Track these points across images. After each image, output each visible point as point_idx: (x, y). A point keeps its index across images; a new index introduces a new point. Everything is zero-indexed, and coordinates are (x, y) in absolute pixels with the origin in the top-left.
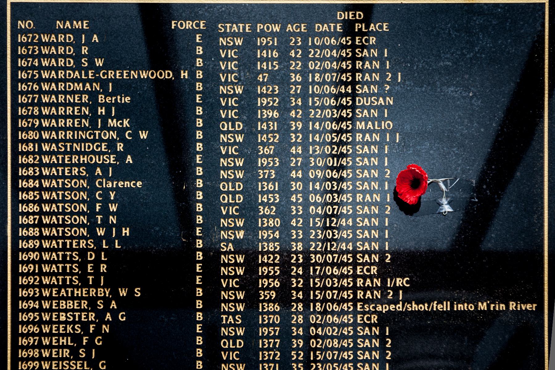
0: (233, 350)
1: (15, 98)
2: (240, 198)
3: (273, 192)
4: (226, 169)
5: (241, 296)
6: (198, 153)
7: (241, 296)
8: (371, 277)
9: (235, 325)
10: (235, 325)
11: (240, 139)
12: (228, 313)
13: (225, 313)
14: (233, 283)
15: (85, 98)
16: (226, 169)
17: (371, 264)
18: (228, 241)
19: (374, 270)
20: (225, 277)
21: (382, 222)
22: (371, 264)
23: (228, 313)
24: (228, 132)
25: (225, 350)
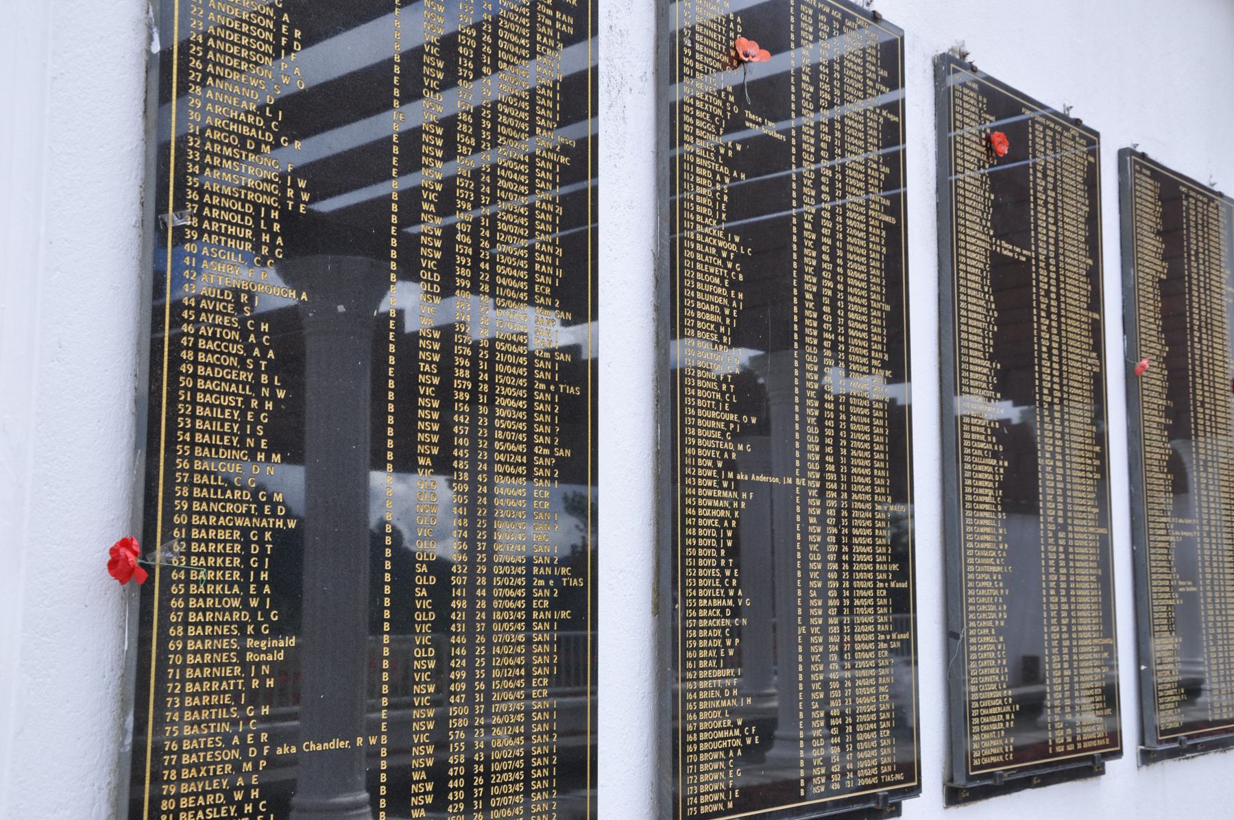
0: (426, 622)
1: (157, 380)
2: (432, 616)
3: (464, 424)
4: (423, 443)
5: (436, 404)
6: (387, 645)
7: (436, 404)
8: (544, 610)
9: (431, 374)
10: (431, 374)
11: (432, 665)
12: (426, 362)
13: (422, 360)
14: (425, 677)
15: (237, 534)
16: (423, 443)
17: (544, 598)
18: (419, 769)
19: (546, 604)
20: (418, 671)
21: (553, 430)
22: (544, 598)
23: (426, 362)
24: (422, 658)
25: (419, 623)
